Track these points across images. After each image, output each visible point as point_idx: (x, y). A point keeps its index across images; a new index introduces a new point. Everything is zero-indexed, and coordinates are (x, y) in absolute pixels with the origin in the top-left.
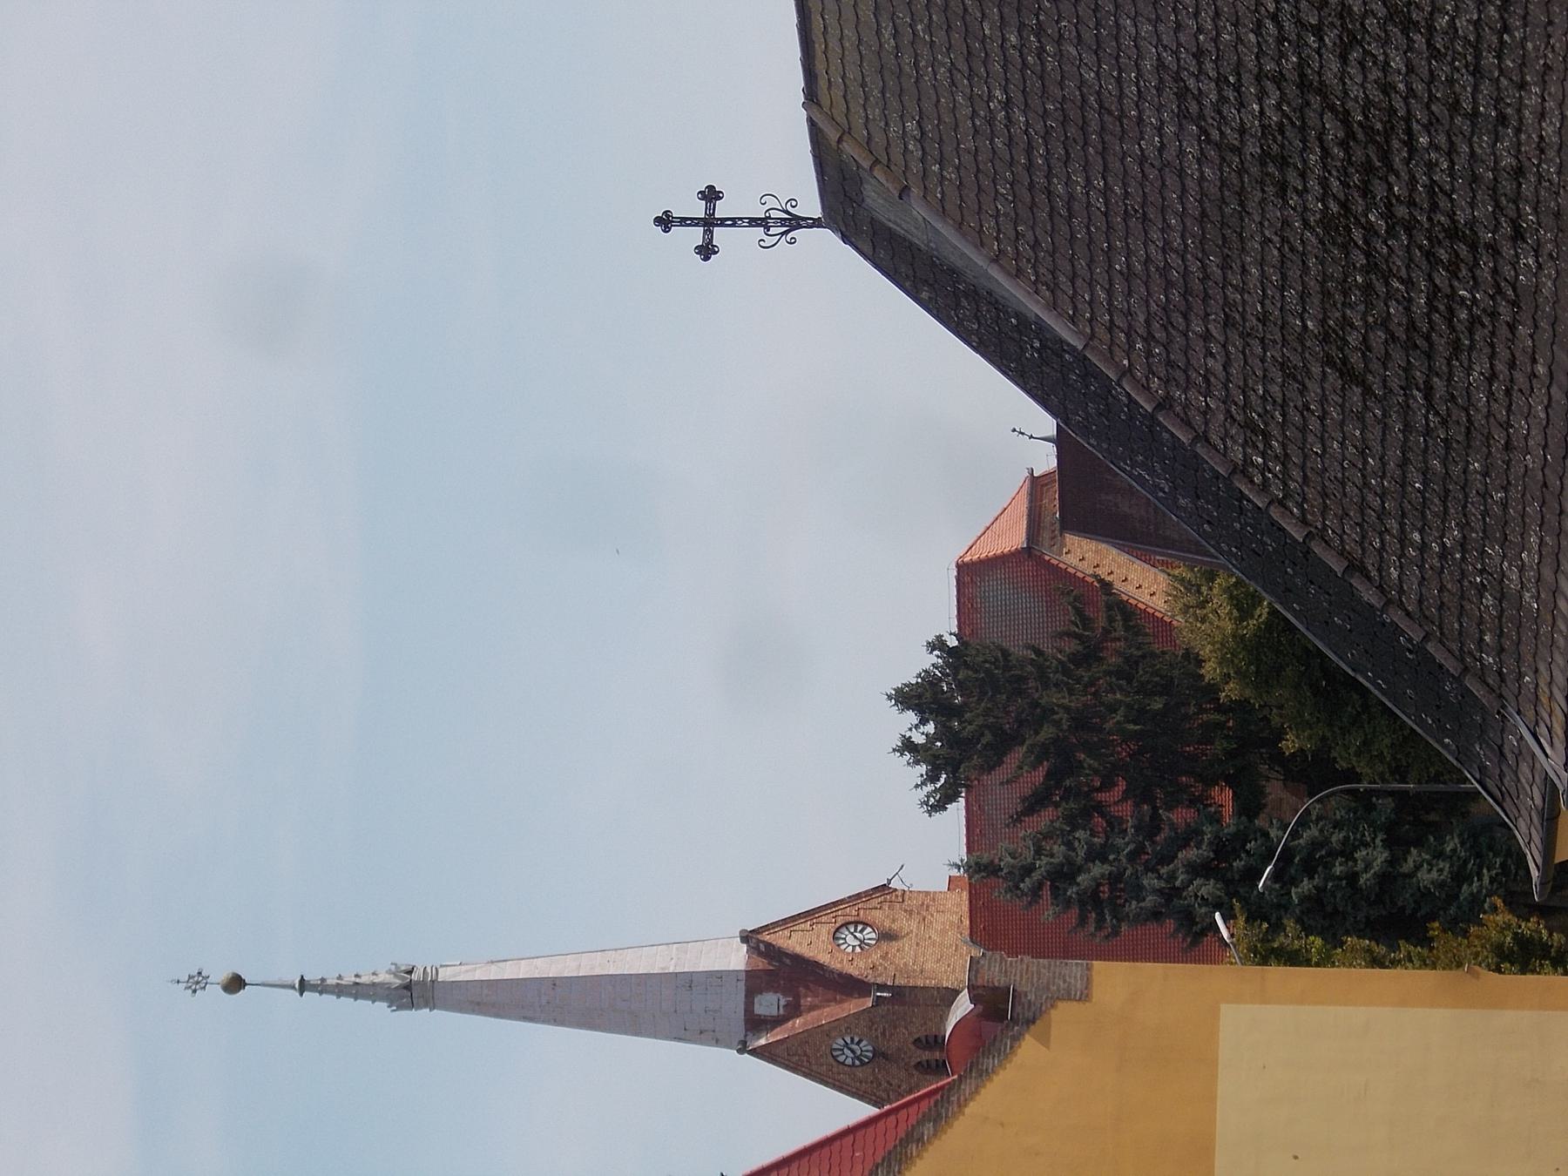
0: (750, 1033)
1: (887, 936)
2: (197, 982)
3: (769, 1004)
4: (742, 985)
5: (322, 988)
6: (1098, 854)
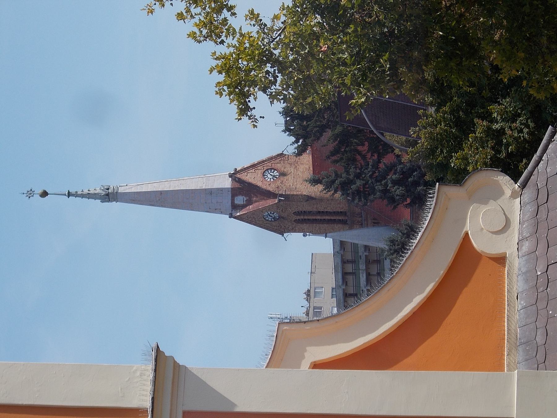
0: (234, 210)
1: (283, 174)
2: (30, 194)
3: (240, 200)
4: (230, 193)
5: (76, 195)
6: (358, 176)
